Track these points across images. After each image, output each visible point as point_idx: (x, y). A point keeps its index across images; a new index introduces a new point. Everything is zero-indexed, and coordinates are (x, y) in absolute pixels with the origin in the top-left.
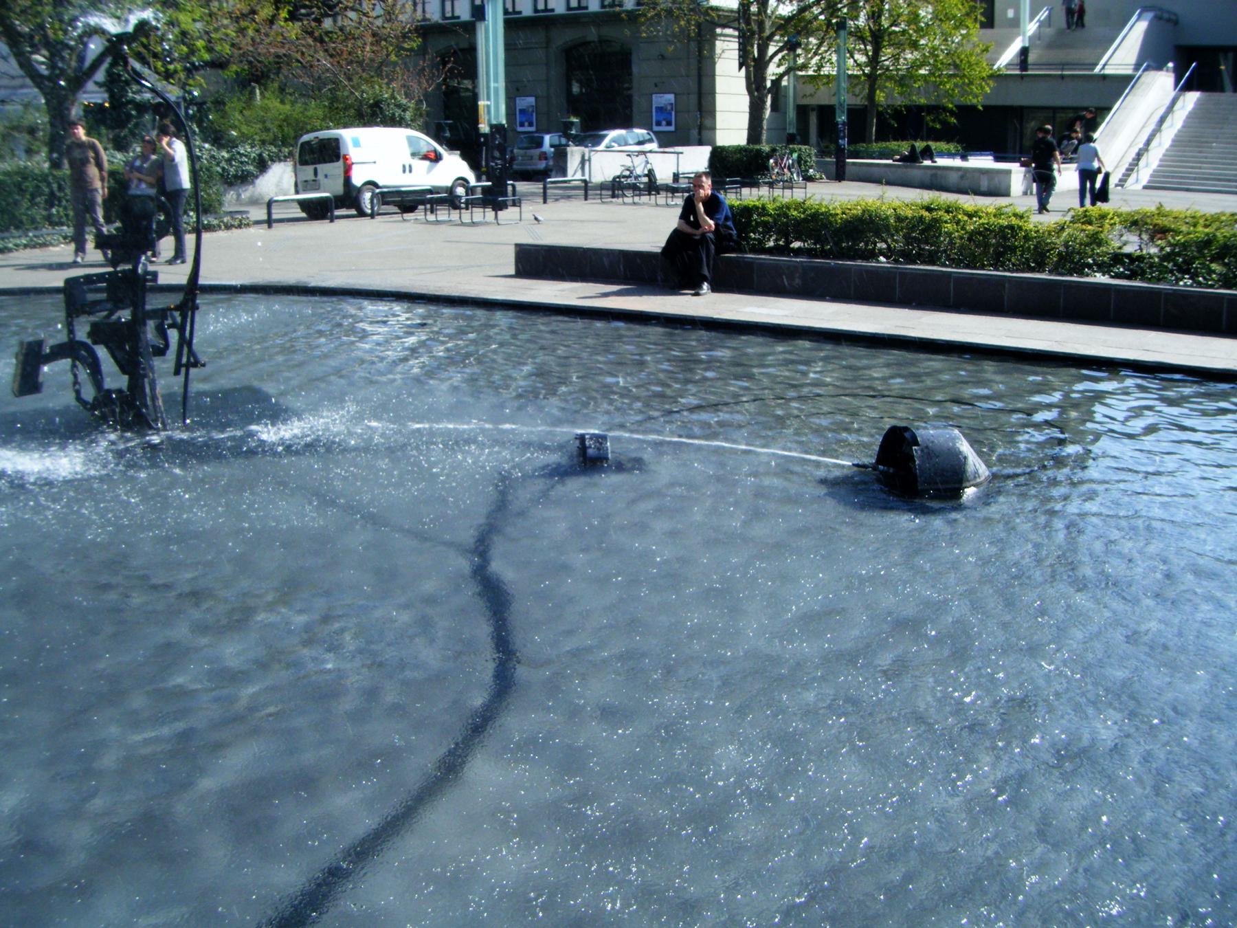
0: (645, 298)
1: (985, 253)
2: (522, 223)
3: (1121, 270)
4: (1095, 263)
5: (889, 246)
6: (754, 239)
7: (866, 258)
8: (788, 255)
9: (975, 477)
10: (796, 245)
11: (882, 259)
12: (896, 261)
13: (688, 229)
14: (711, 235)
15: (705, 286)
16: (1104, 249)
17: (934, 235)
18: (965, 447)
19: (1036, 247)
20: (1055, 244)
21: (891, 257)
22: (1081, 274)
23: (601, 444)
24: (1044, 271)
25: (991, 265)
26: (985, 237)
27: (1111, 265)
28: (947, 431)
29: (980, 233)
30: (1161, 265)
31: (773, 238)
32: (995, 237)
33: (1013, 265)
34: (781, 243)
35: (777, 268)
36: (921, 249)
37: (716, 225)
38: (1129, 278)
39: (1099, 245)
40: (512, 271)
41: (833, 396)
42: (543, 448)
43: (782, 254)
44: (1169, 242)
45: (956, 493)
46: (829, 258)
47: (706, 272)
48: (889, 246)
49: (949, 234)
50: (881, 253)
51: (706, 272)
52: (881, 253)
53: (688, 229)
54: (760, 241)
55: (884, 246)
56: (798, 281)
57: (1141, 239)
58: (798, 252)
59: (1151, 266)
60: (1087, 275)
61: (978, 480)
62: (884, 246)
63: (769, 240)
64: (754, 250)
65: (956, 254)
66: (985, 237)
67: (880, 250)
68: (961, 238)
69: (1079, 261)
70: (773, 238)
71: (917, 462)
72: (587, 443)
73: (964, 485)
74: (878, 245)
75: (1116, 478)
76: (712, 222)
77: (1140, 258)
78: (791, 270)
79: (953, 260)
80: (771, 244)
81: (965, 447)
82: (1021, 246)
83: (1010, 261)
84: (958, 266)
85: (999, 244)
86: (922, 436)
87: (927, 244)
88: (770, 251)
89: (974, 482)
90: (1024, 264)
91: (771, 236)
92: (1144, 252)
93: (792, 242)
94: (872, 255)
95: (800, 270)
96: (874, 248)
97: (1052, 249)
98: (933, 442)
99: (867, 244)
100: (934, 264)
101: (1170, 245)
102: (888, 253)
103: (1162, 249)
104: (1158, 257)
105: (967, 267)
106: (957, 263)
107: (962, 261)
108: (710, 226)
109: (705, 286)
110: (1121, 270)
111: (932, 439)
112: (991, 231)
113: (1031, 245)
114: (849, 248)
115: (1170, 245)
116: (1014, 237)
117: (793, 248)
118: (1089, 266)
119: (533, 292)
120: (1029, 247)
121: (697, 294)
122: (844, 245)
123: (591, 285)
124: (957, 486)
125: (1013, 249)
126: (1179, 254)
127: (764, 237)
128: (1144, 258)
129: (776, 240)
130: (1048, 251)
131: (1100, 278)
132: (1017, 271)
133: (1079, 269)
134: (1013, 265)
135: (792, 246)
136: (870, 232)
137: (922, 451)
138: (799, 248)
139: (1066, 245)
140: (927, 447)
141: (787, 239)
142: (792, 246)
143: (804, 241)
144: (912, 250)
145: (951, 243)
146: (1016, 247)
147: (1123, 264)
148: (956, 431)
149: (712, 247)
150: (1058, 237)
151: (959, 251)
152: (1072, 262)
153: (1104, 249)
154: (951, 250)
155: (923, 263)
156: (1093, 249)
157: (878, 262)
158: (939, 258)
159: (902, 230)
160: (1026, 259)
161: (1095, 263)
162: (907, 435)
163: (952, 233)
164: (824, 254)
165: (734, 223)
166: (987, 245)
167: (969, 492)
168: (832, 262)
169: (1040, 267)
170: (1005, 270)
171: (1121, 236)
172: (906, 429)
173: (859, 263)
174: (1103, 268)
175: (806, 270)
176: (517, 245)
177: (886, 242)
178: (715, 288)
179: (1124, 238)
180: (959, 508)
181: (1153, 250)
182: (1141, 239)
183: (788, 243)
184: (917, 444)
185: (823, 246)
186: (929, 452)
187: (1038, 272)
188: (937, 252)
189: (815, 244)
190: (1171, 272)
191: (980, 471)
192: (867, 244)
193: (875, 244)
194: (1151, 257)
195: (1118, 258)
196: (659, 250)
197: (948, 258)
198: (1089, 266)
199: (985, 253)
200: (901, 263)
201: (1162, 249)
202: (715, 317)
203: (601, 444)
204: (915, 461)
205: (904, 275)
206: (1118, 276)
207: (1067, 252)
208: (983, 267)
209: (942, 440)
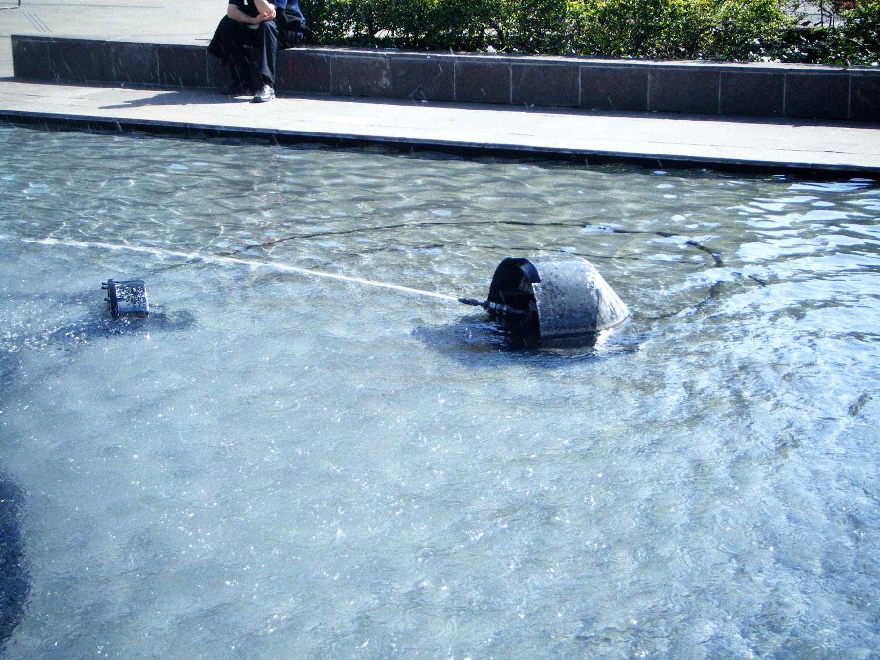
0: (190, 106)
1: (620, 37)
2: (21, 8)
3: (797, 51)
4: (763, 44)
5: (500, 32)
6: (329, 28)
7: (471, 49)
8: (373, 48)
9: (612, 318)
10: (382, 34)
11: (491, 49)
12: (509, 52)
13: (243, 17)
14: (272, 24)
15: (268, 89)
16: (774, 25)
17: (557, 17)
18: (600, 283)
19: (686, 26)
20: (710, 21)
21: (503, 46)
22: (744, 58)
23: (136, 294)
24: (696, 57)
25: (629, 53)
26: (620, 16)
27: (783, 46)
28: (574, 262)
29: (614, 12)
30: (848, 41)
31: (353, 26)
32: (634, 16)
33: (658, 51)
34: (363, 32)
35: (359, 65)
36: (541, 35)
37: (278, 10)
38: (806, 61)
39: (768, 20)
40: (11, 73)
41: (509, 223)
42: (454, 180)
43: (364, 46)
44: (859, 11)
45: (589, 339)
46: (424, 50)
47: (267, 72)
48: (500, 32)
49: (576, 15)
50: (491, 42)
51: (267, 72)
52: (491, 42)
53: (243, 17)
54: (336, 30)
55: (494, 33)
56: (385, 81)
57: (823, 9)
58: (385, 43)
59: (835, 44)
60: (752, 60)
61: (616, 322)
62: (494, 33)
63: (347, 28)
64: (329, 43)
65: (584, 39)
66: (620, 16)
67: (489, 38)
68: (591, 19)
69: (742, 42)
70: (353, 26)
71: (538, 302)
72: (118, 295)
73: (598, 328)
74: (486, 31)
75: (220, 212)
76: (272, 7)
77: (821, 34)
78: (376, 67)
79: (582, 47)
80: (351, 33)
81: (600, 283)
82: (667, 26)
83: (653, 46)
84: (587, 55)
85: (640, 26)
86: (543, 270)
87: (547, 27)
88: (351, 43)
89: (611, 324)
90: (671, 49)
91: (350, 23)
92: (826, 26)
93: (377, 31)
94: (479, 44)
95: (388, 67)
96: (481, 36)
97: (709, 27)
98: (557, 276)
99: (471, 32)
100: (557, 54)
101: (861, 15)
102: (499, 43)
103: (850, 20)
104: (845, 32)
105: (600, 55)
106: (587, 51)
107: (592, 49)
108: (270, 12)
109: (268, 89)
110: (797, 51)
111: (555, 272)
112: (629, 9)
113: (680, 23)
114: (450, 37)
115: (861, 15)
116: (658, 16)
117: (378, 39)
118: (755, 49)
119: (40, 100)
120: (678, 27)
121: (257, 101)
122: (442, 32)
123: (117, 90)
124: (590, 330)
125: (657, 31)
126: (872, 26)
127: (341, 24)
128: (826, 34)
129: (357, 29)
130: (702, 31)
131: (768, 63)
132: (663, 58)
133: (743, 52)
134: (658, 51)
135: (377, 35)
136: (475, 15)
137: (544, 288)
138: (386, 38)
139: (725, 21)
140: (550, 283)
141: (370, 27)
142: (377, 35)
143: (392, 29)
144: (529, 37)
145: (579, 26)
146: (661, 28)
147: (799, 43)
148: (586, 262)
149: (275, 40)
150: (715, 13)
151: (589, 35)
152: (734, 44)
153: (774, 25)
154: (579, 34)
155: (544, 52)
156: (759, 27)
157: (486, 53)
158: (563, 46)
159: (515, 11)
160: (674, 42)
161: (763, 44)
162: (524, 268)
163: (578, 14)
164: (420, 46)
165: (301, 6)
166: (623, 27)
167: (603, 338)
168: (429, 55)
169: (691, 53)
170: (647, 58)
171: (797, 7)
172: (523, 261)
173: (462, 55)
174: (771, 49)
175: (395, 65)
176: (14, 37)
177: (496, 27)
178: (281, 92)
179: (801, 10)
180: (595, 358)
181: (838, 24)
182: (823, 9)
183: (372, 32)
184: (537, 280)
185: (416, 35)
186: (553, 289)
187: (689, 58)
188: (560, 38)
189: (406, 32)
190: (862, 50)
191: (618, 311)
192: (471, 32)
193: (482, 30)
194: (835, 32)
195: (791, 36)
196: (207, 45)
197: (575, 46)
198: (755, 49)
199: (620, 37)
200: (515, 54)
201: (850, 20)
202: (281, 128)
203: (136, 294)
204: (535, 301)
205: (519, 68)
206: (791, 59)
207: (726, 32)
208: (619, 55)
209: (568, 273)
